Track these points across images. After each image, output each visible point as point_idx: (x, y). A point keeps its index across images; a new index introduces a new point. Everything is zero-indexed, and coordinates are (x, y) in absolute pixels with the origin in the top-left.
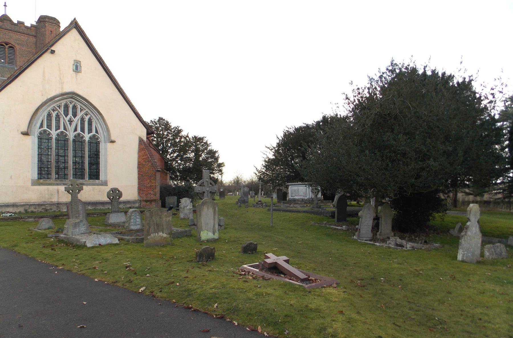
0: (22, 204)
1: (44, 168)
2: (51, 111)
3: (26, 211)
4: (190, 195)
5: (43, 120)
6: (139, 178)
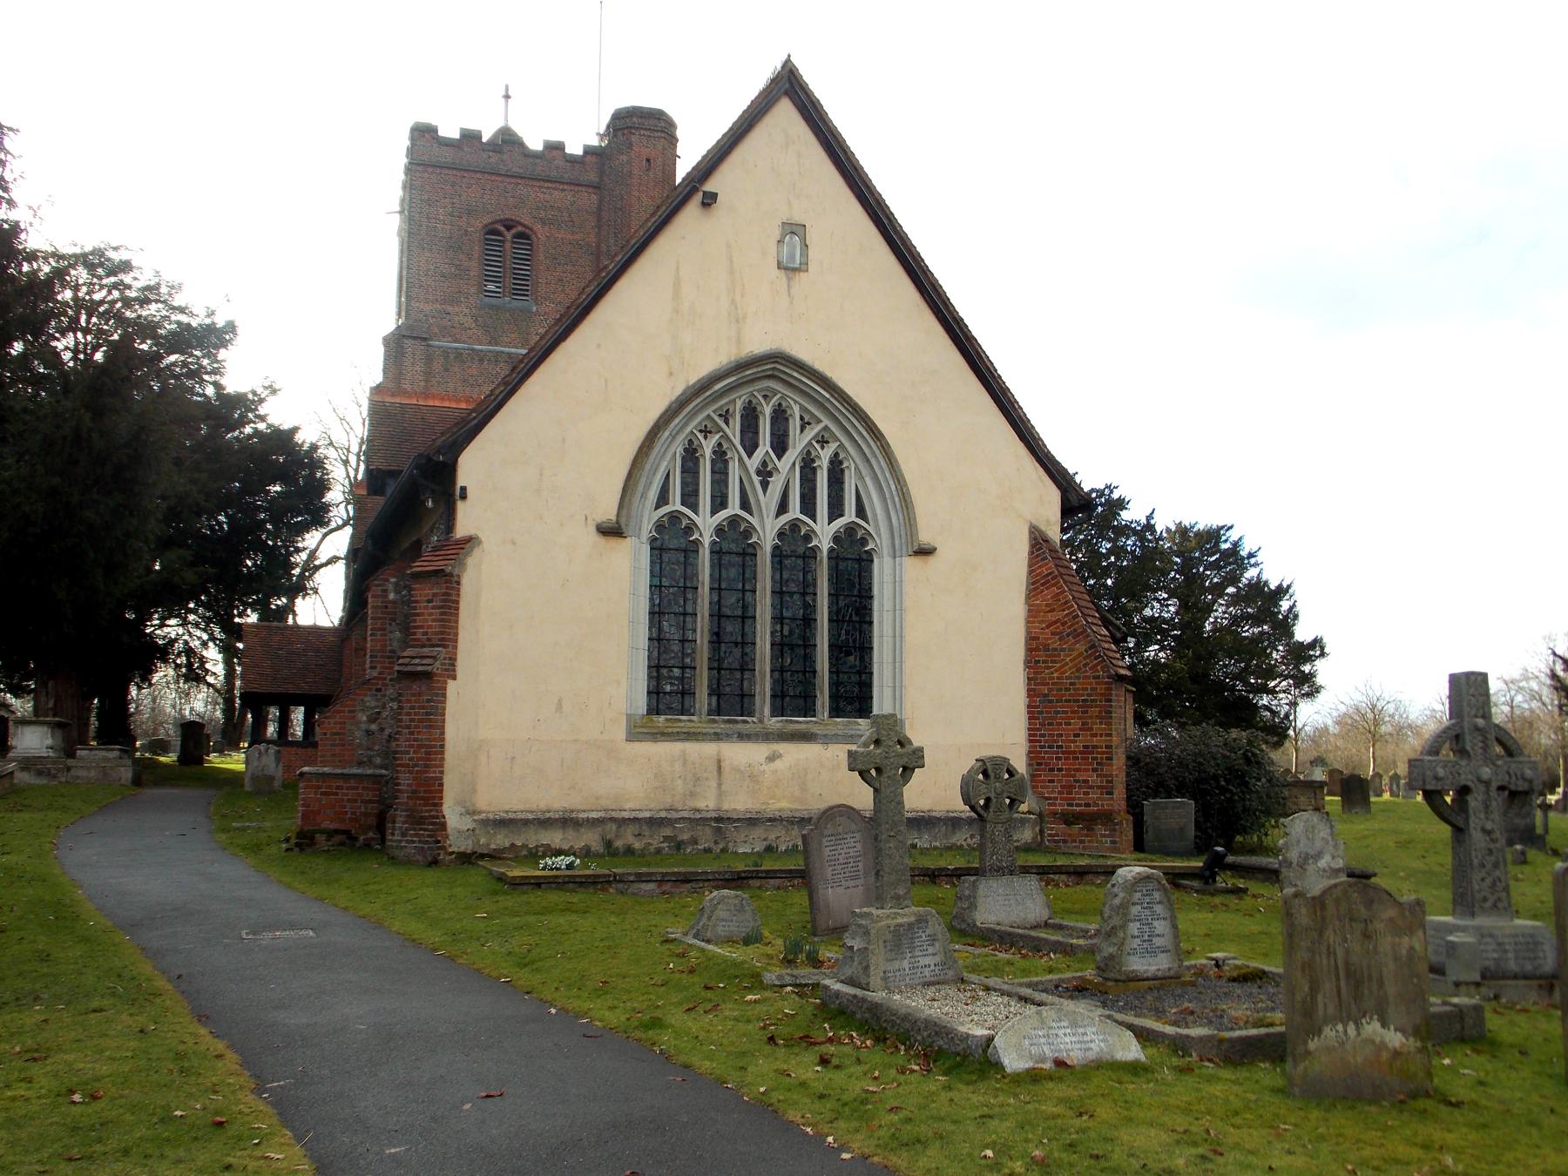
0: (594, 815)
1: (670, 668)
2: (698, 434)
3: (608, 844)
4: (1255, 796)
5: (668, 475)
6: (1032, 715)
